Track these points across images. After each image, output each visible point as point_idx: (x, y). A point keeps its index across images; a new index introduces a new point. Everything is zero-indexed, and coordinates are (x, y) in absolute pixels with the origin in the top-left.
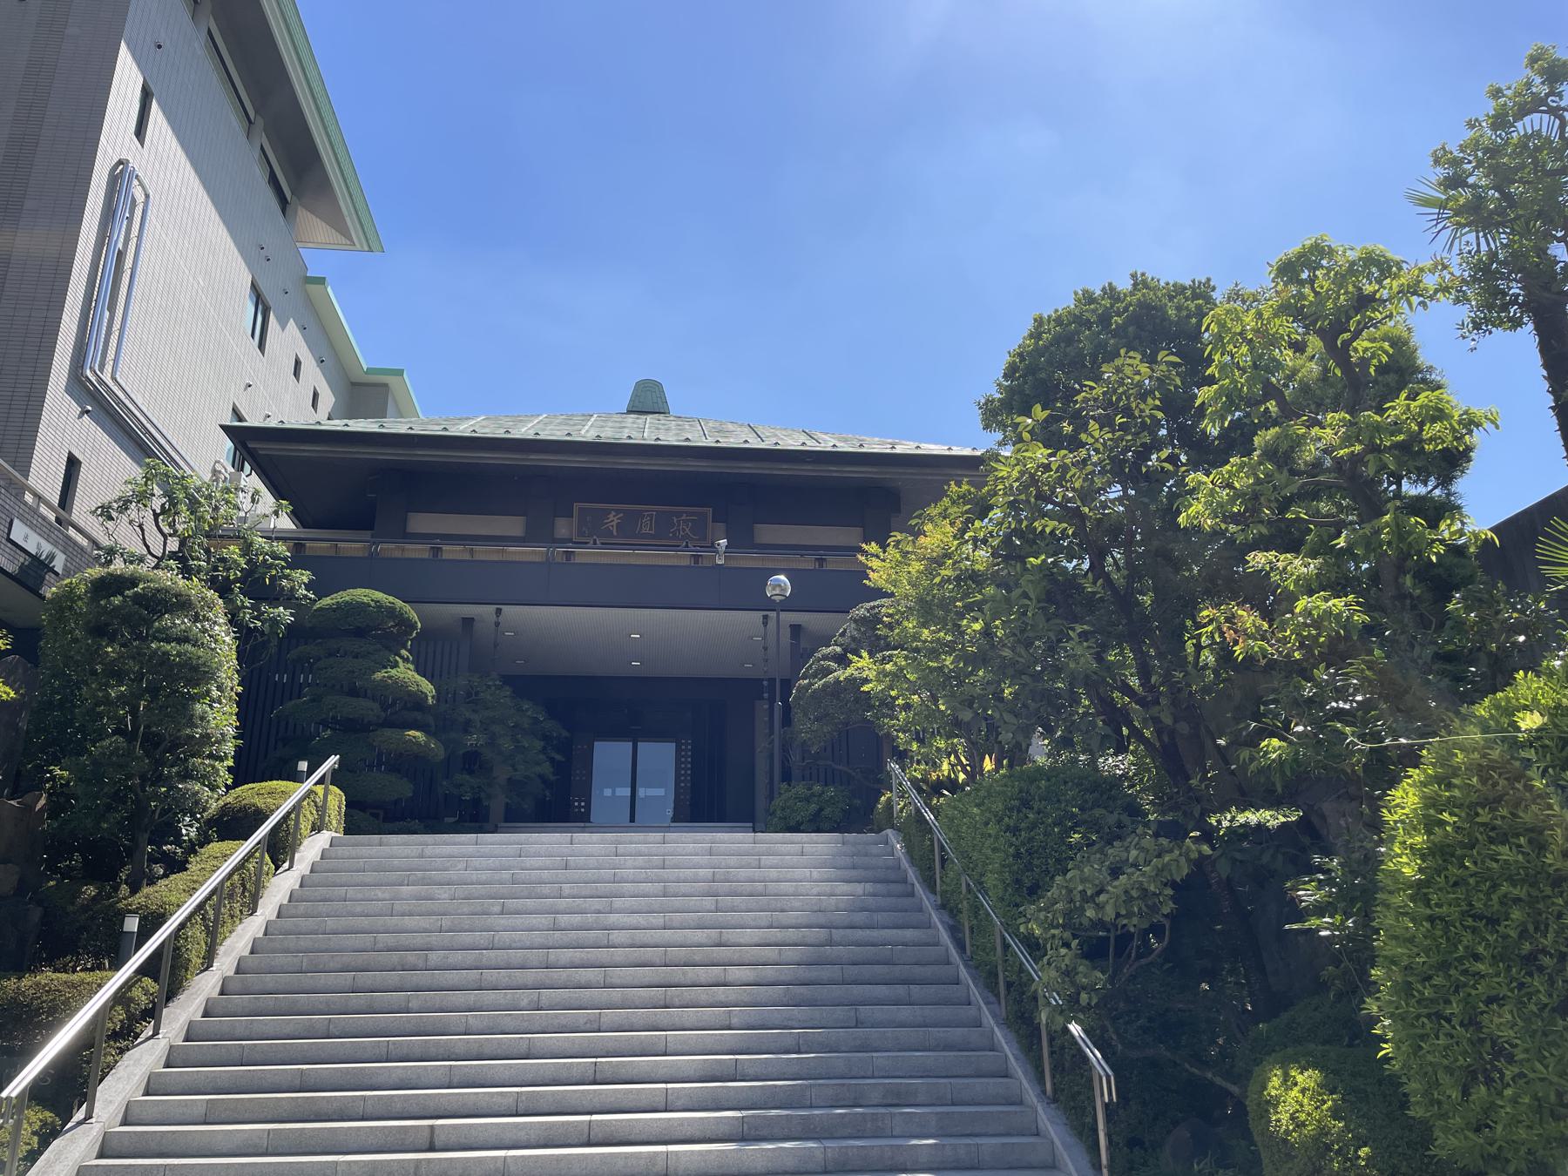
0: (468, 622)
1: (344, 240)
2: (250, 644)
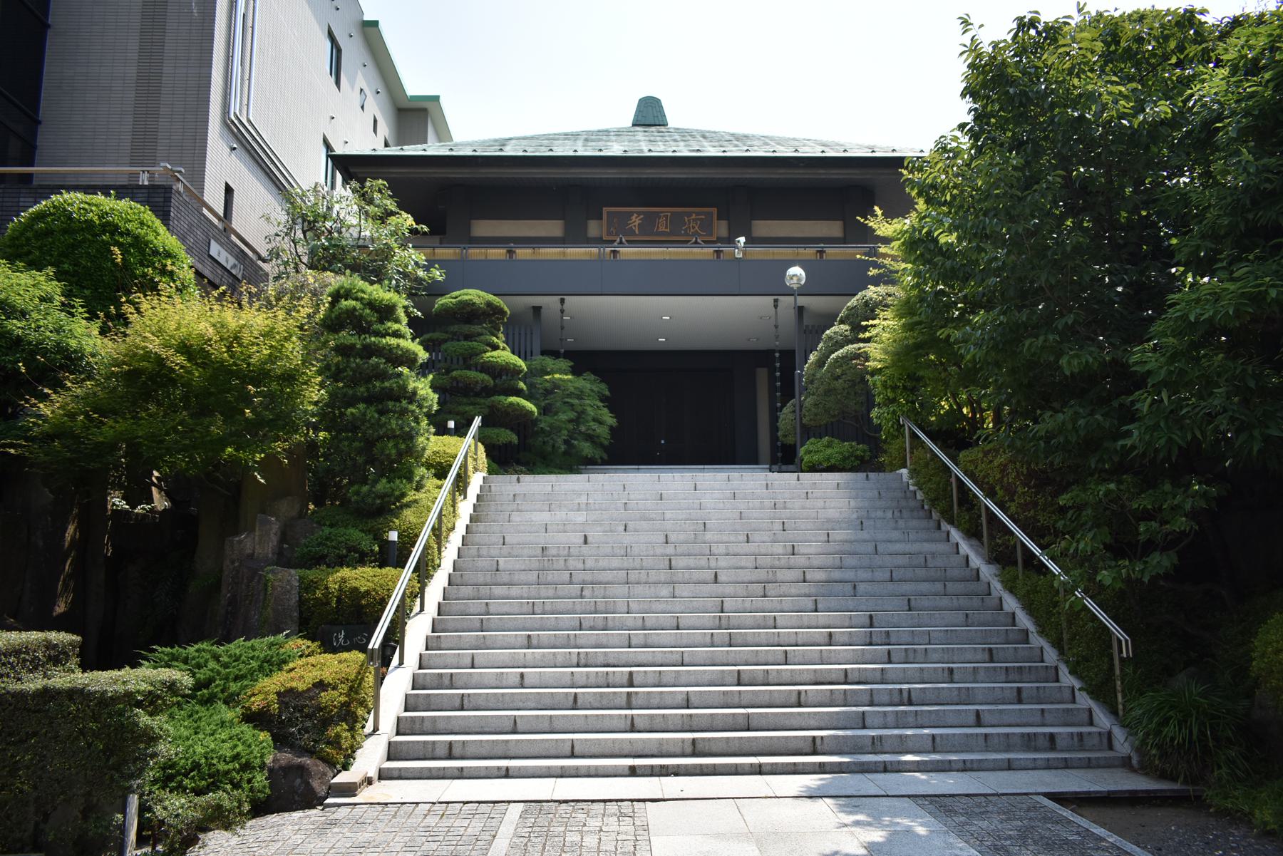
0: (537, 310)
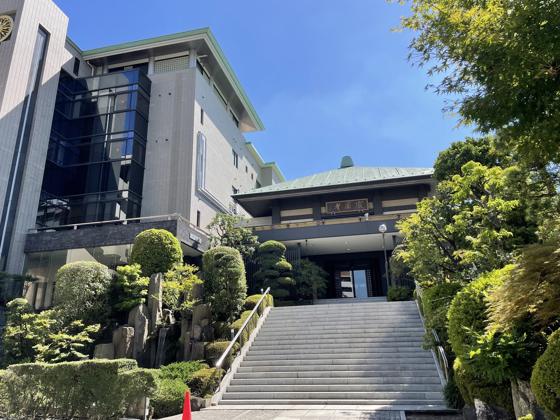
0: (299, 244)
1: (254, 129)
2: (246, 259)
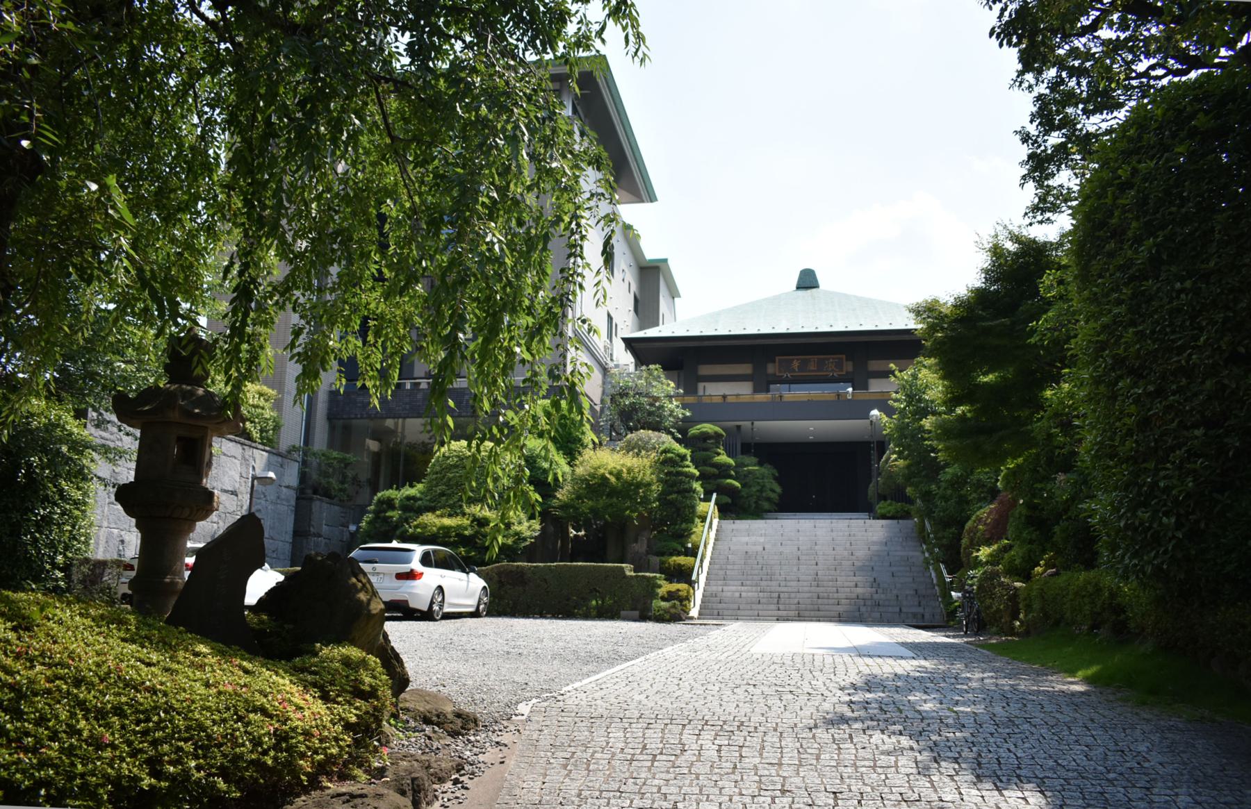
0: (739, 427)
